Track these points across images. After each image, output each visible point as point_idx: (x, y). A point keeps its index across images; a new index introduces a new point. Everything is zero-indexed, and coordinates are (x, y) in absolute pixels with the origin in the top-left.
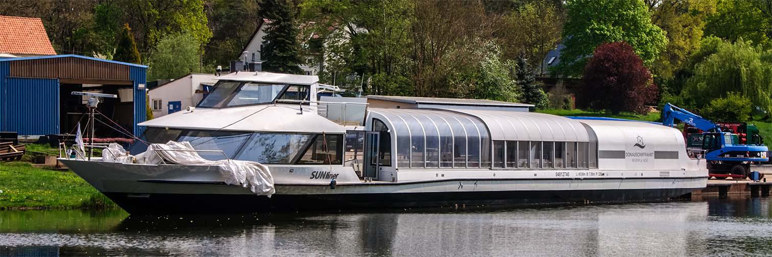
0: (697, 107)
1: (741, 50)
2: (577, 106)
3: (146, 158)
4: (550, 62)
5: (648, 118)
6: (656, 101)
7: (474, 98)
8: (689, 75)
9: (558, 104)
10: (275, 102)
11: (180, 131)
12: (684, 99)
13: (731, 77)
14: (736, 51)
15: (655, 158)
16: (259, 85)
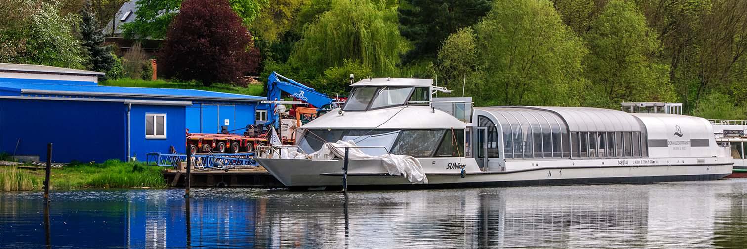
1: (360, 7)
2: (159, 75)
4: (123, 19)
6: (258, 70)
7: (25, 62)
8: (297, 37)
9: (135, 72)
10: (407, 104)
12: (292, 68)
13: (349, 41)
14: (354, 8)
15: (691, 146)
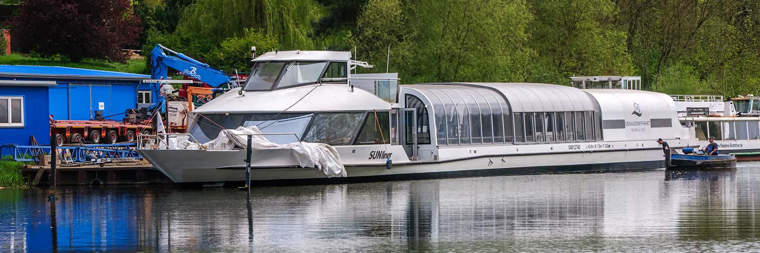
0: (201, 51)
3: (219, 144)
5: (127, 67)
12: (182, 39)
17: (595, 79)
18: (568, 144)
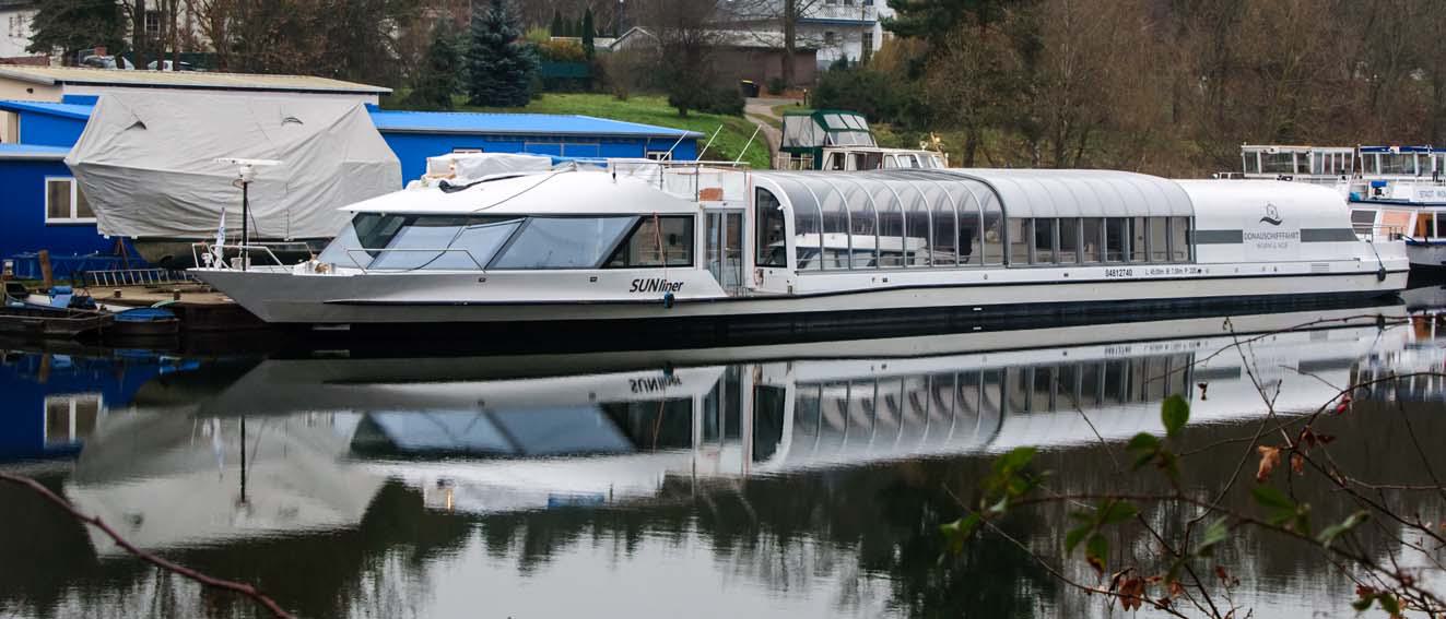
11: (402, 219)
16: (257, 234)
17: (1272, 150)
18: (1106, 268)
